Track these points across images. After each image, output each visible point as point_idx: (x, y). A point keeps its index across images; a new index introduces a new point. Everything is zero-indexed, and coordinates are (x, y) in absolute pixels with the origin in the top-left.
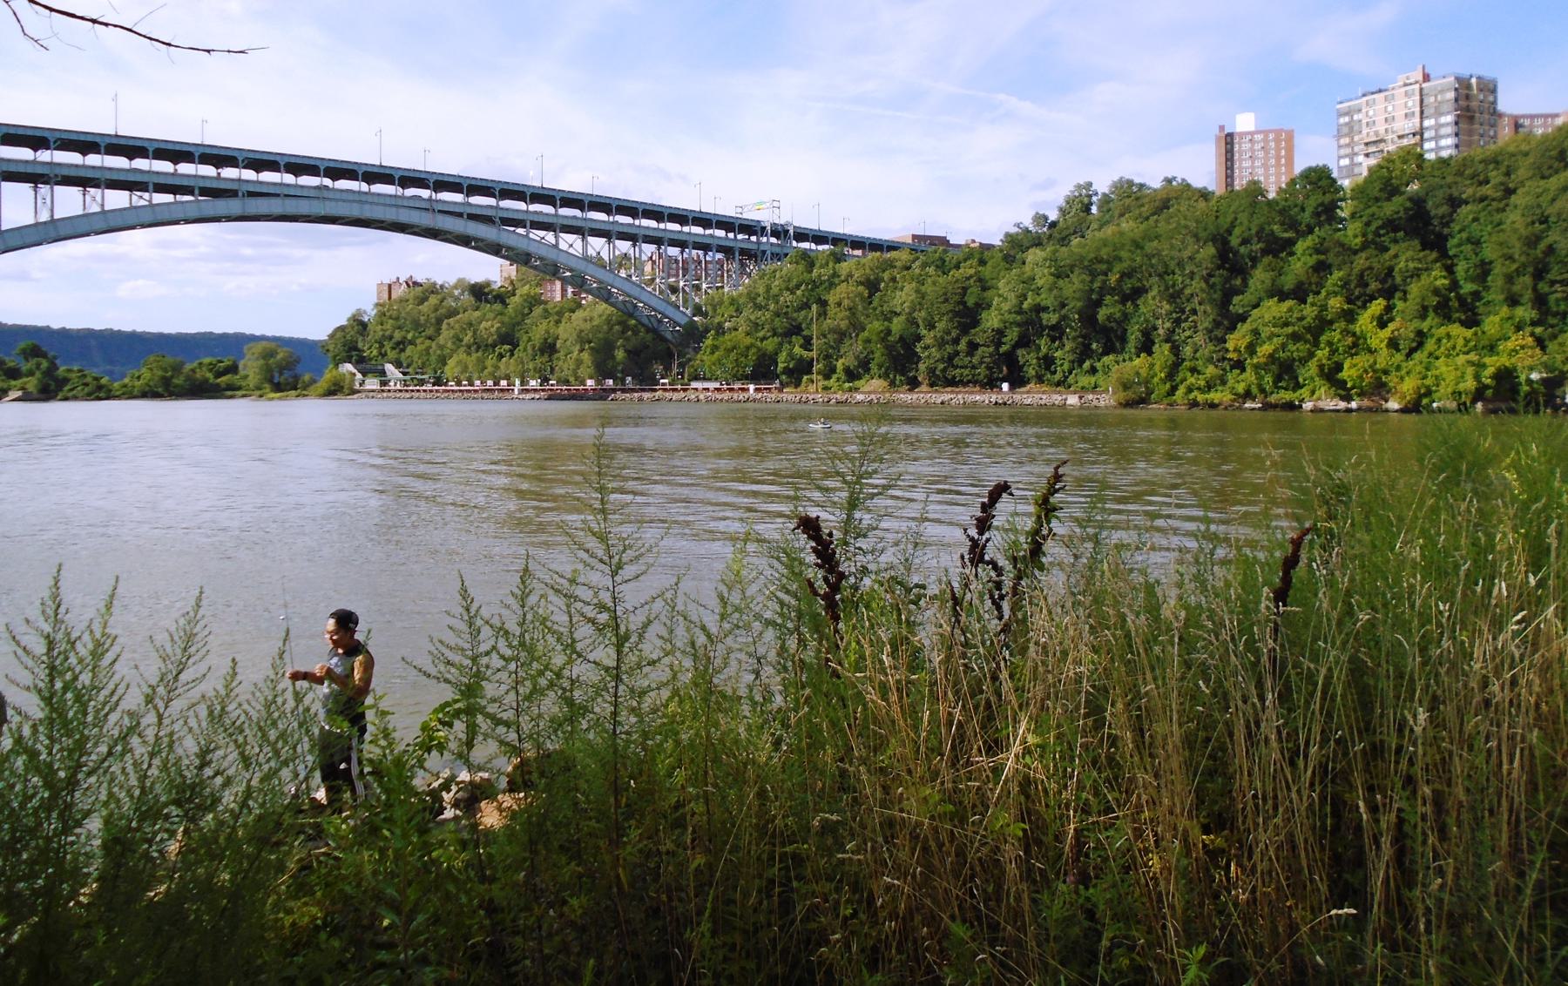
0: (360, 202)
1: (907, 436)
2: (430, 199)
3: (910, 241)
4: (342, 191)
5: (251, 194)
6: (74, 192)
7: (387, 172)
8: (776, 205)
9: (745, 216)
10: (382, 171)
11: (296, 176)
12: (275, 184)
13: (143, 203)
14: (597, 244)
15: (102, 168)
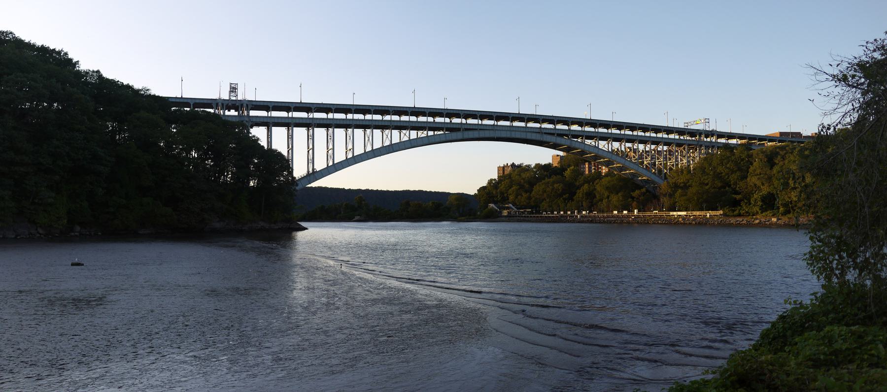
0: (510, 130)
1: (318, 259)
2: (494, 125)
3: (779, 136)
4: (486, 125)
5: (467, 129)
6: (395, 133)
7: (522, 116)
8: (707, 121)
9: (689, 127)
10: (519, 116)
11: (417, 117)
12: (475, 124)
13: (423, 135)
14: (616, 145)
15: (372, 120)
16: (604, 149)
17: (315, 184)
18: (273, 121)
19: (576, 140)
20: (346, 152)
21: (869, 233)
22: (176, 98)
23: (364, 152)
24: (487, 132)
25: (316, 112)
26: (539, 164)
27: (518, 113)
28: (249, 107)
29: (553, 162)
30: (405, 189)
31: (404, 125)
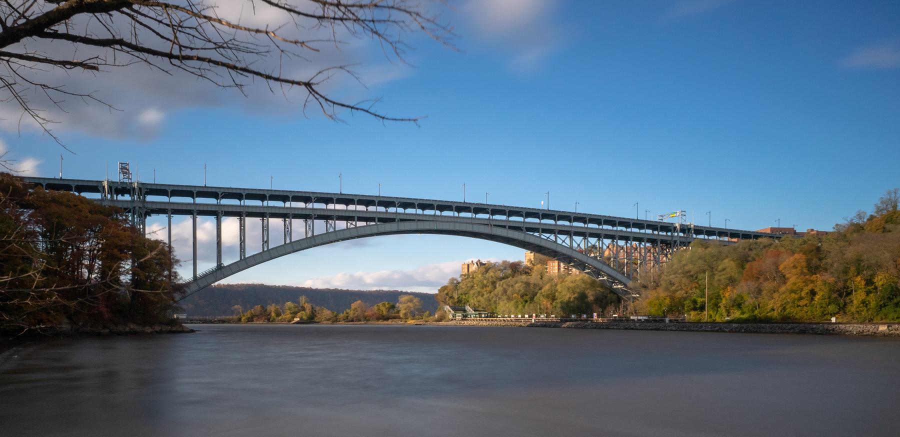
9: (665, 221)
16: (564, 244)
17: (224, 282)
18: (337, 214)
19: (532, 233)
20: (263, 244)
21: (13, 319)
22: (55, 179)
23: (283, 243)
24: (428, 223)
25: (316, 202)
26: (506, 261)
27: (378, 195)
28: (143, 192)
29: (174, 241)
30: (288, 285)
31: (329, 214)
